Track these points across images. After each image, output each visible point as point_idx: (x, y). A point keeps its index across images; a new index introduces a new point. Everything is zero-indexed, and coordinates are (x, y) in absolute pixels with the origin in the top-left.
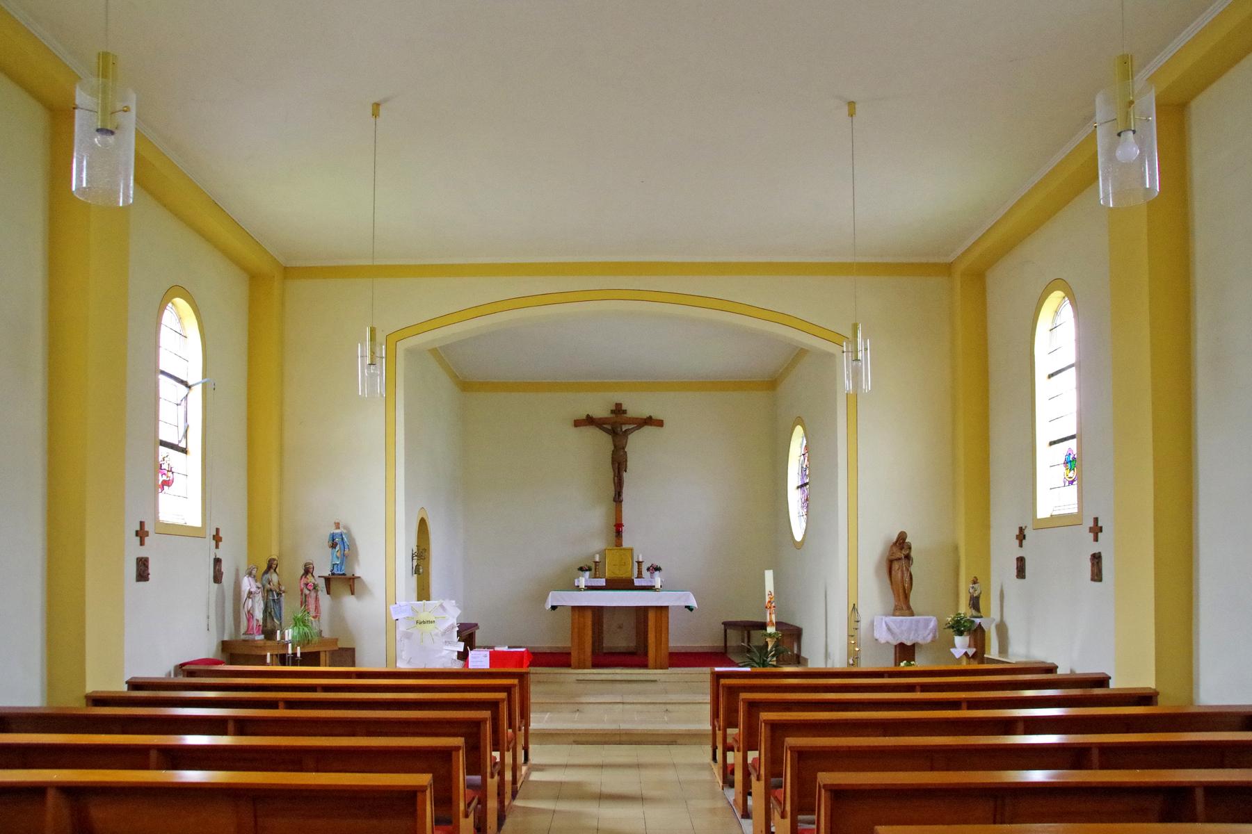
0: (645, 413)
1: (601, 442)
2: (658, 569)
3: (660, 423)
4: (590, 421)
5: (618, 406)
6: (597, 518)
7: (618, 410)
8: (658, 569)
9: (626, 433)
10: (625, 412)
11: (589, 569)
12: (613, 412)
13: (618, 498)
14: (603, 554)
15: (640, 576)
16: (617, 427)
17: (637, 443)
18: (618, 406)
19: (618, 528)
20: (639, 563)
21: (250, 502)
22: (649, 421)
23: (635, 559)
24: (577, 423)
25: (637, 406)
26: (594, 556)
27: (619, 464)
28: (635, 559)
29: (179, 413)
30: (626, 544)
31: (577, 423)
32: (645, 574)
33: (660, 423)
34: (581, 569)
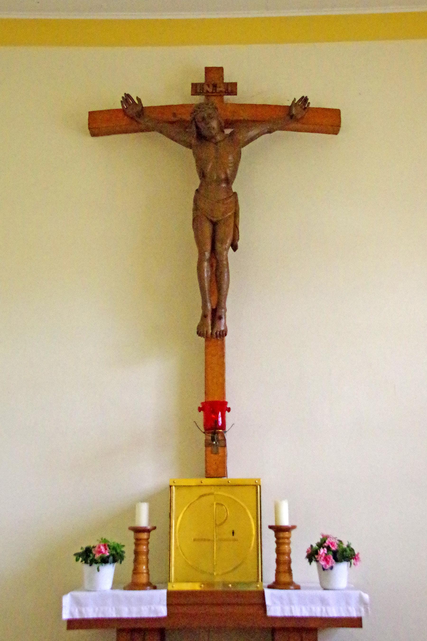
0: (285, 95)
1: (162, 172)
2: (344, 555)
3: (329, 122)
4: (129, 118)
5: (214, 73)
6: (149, 390)
7: (214, 85)
8: (344, 555)
9: (236, 145)
10: (232, 89)
11: (116, 556)
12: (196, 89)
13: (212, 327)
14: (162, 501)
15: (283, 580)
16: (211, 128)
17: (271, 177)
18: (214, 73)
19: (214, 414)
20: (279, 530)
21: (184, 486)
22: (304, 117)
23: (268, 520)
24: (100, 124)
25: (263, 76)
26: (132, 511)
27: (215, 230)
28: (268, 520)
29: (224, 494)
30: (235, 470)
31: (100, 124)
32: (303, 570)
33: (329, 122)
34: (87, 556)
